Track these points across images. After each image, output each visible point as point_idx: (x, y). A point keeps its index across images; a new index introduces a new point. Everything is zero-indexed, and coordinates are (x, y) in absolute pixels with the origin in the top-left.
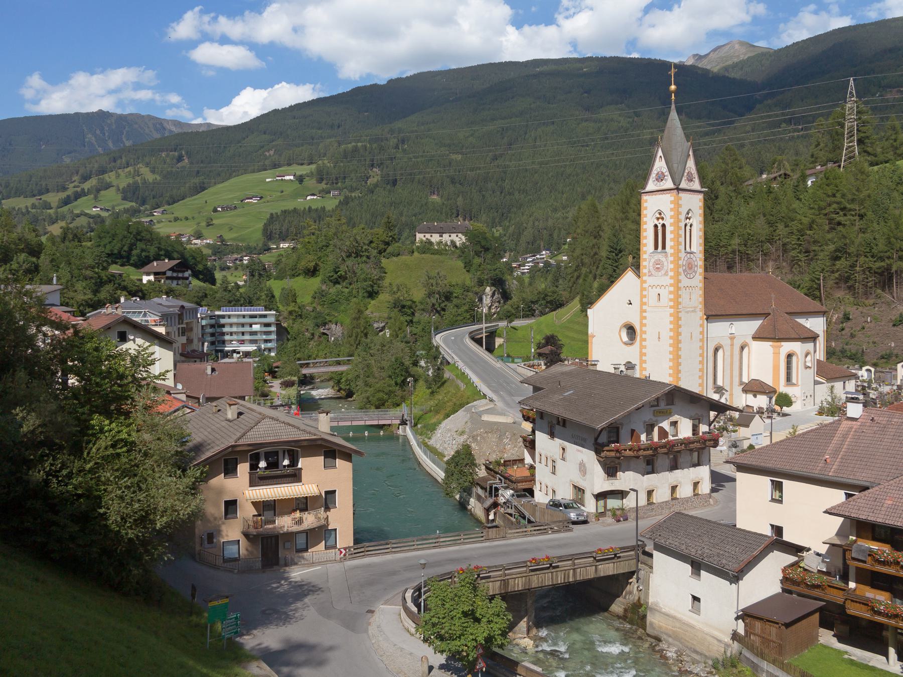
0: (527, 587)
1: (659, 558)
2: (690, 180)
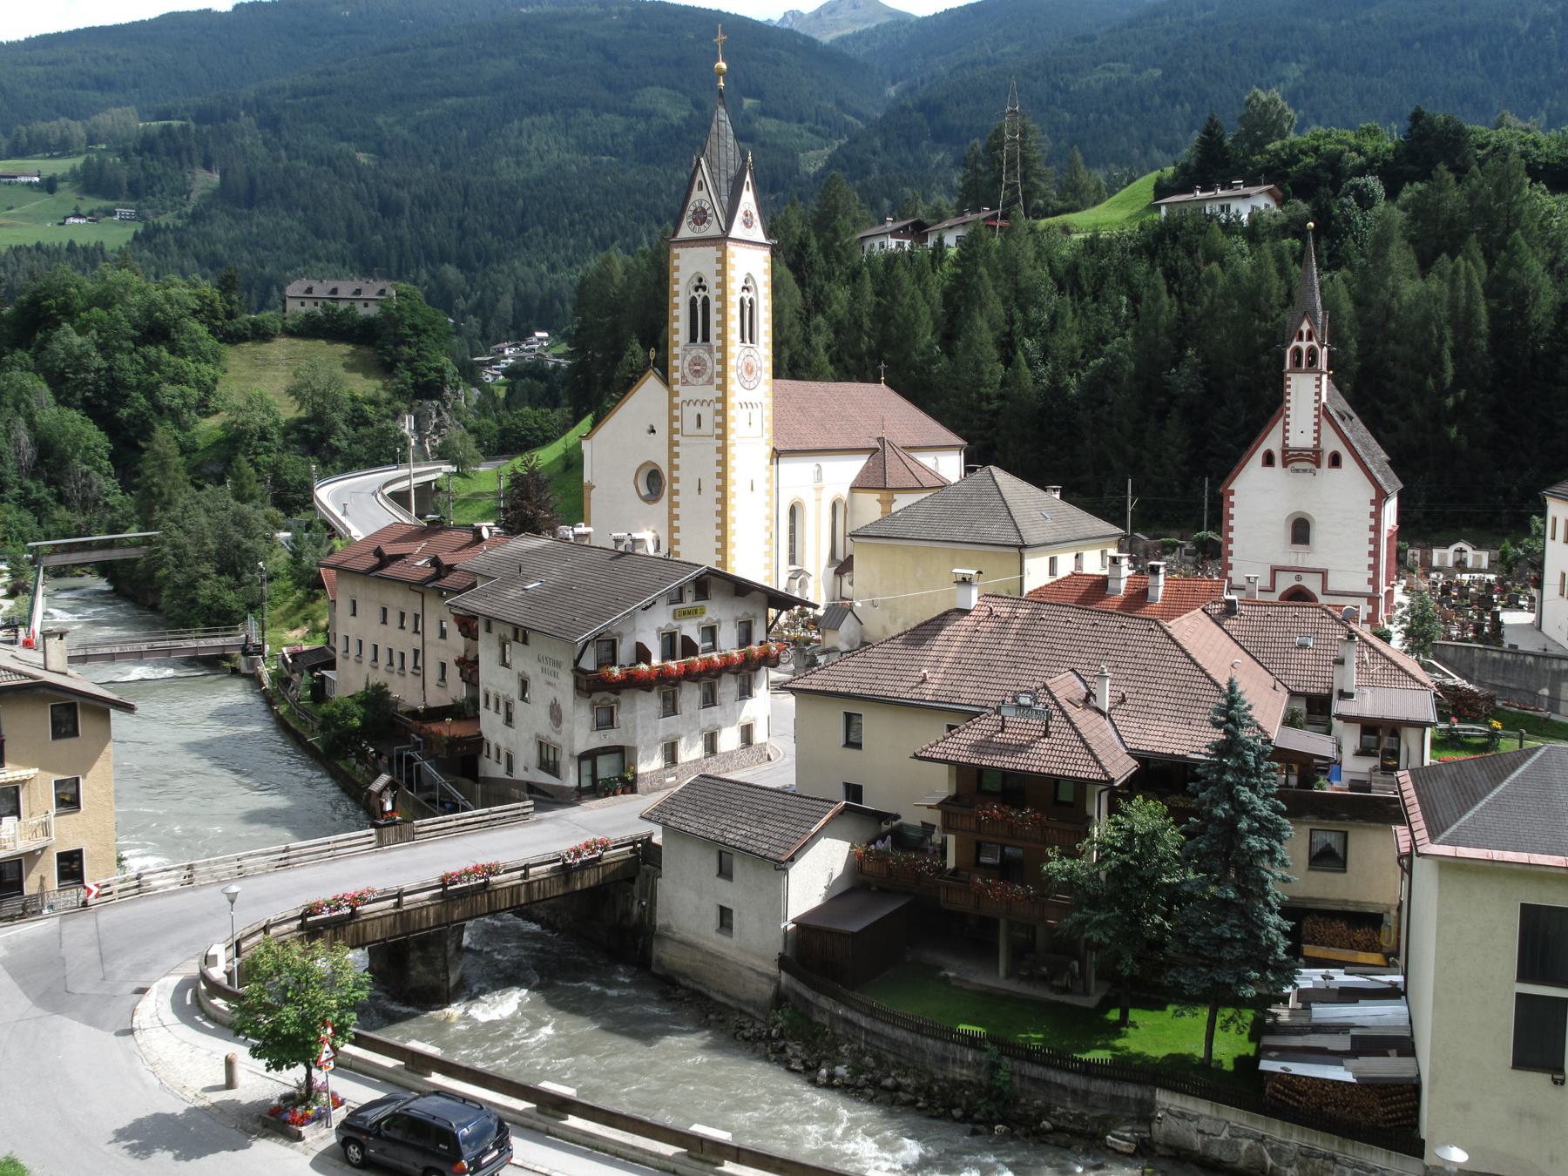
0: (444, 921)
2: (748, 224)
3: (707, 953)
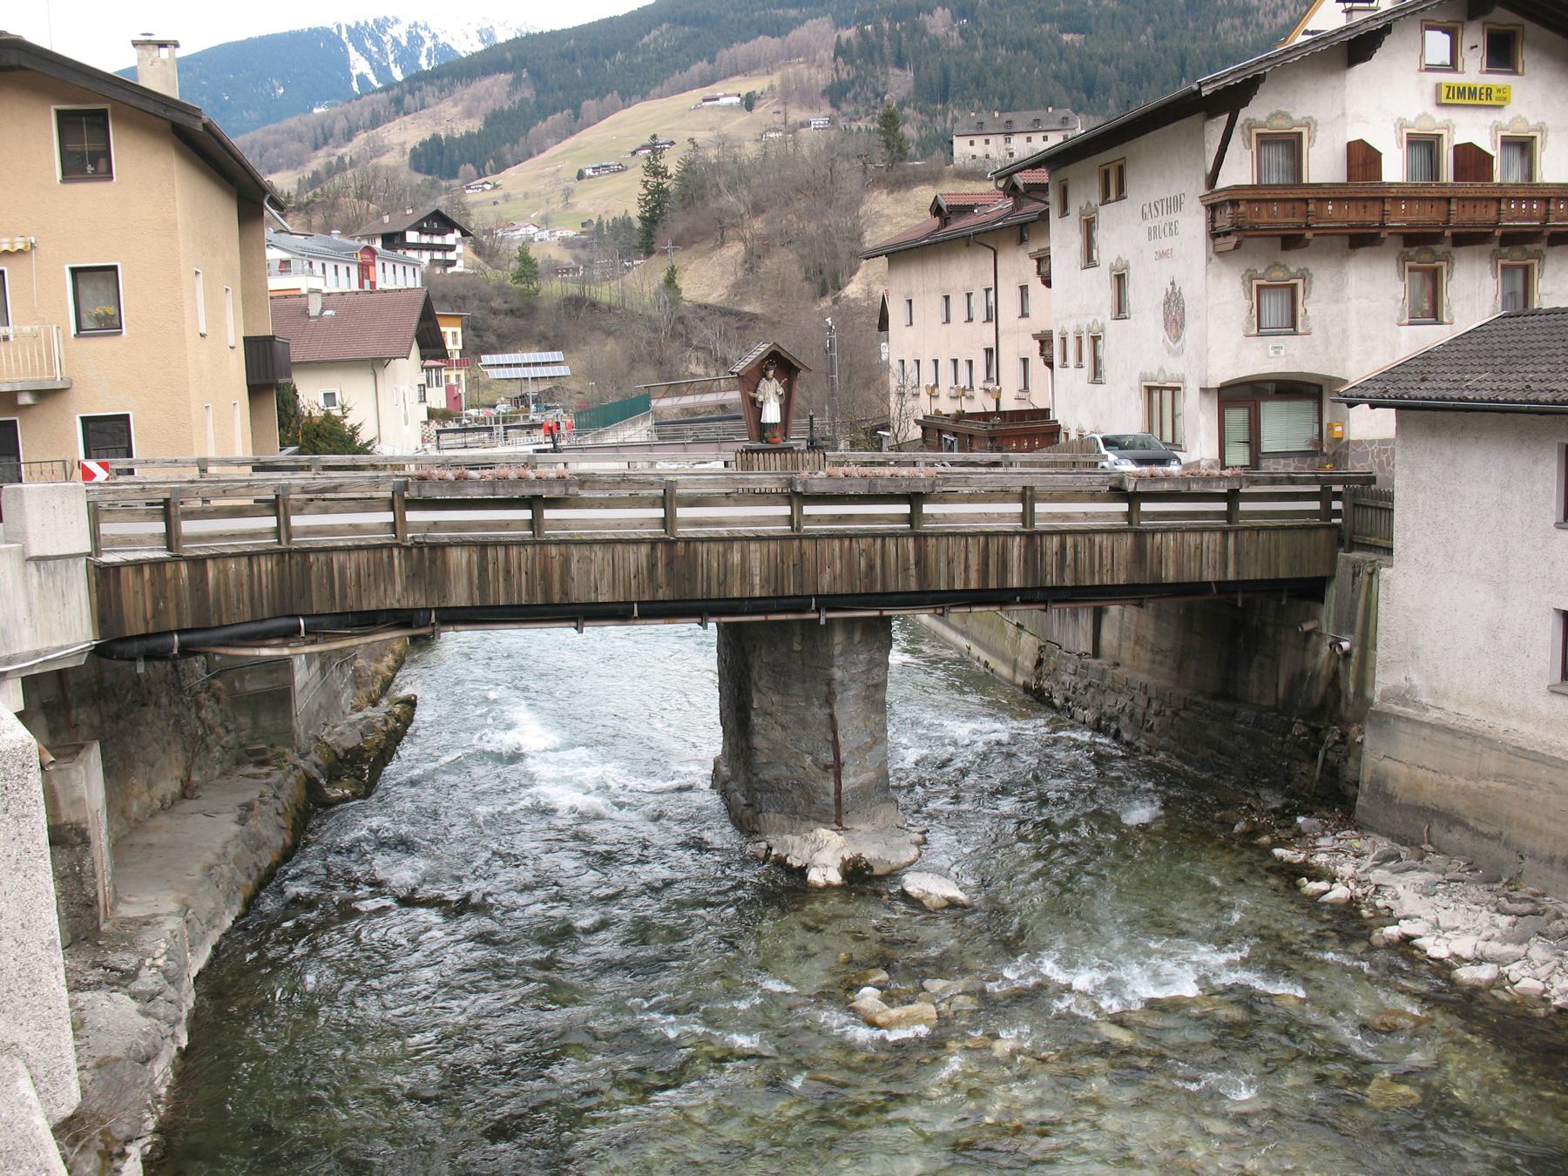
1: (1345, 181)
3: (1521, 753)
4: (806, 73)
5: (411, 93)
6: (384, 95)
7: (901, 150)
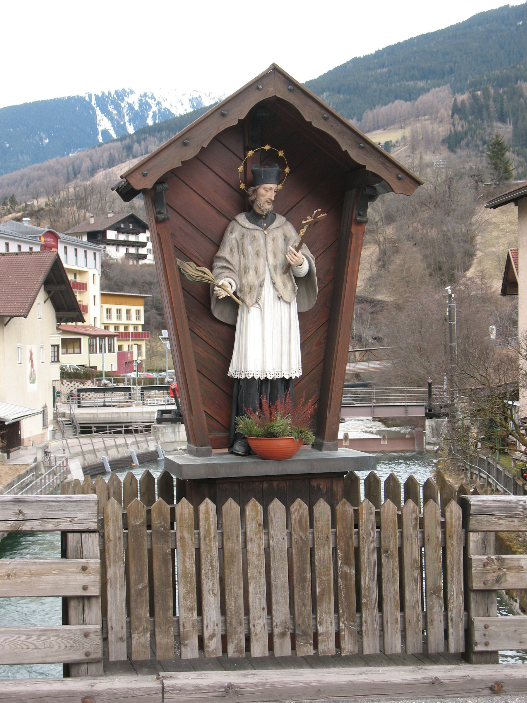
4: (430, 127)
5: (139, 142)
6: (119, 144)
7: (507, 171)
